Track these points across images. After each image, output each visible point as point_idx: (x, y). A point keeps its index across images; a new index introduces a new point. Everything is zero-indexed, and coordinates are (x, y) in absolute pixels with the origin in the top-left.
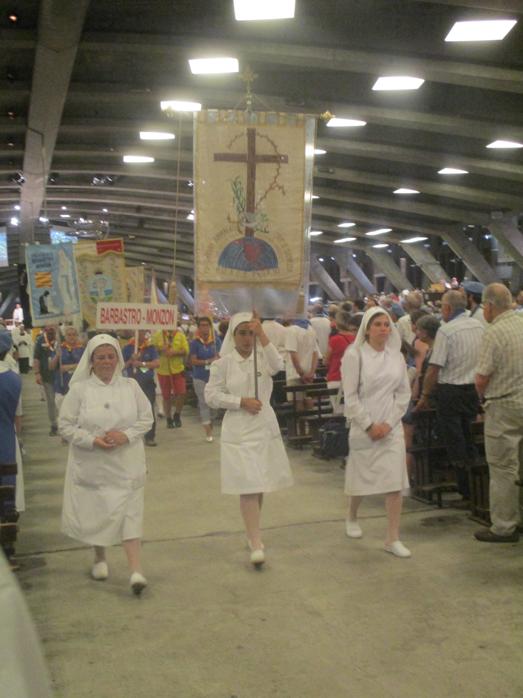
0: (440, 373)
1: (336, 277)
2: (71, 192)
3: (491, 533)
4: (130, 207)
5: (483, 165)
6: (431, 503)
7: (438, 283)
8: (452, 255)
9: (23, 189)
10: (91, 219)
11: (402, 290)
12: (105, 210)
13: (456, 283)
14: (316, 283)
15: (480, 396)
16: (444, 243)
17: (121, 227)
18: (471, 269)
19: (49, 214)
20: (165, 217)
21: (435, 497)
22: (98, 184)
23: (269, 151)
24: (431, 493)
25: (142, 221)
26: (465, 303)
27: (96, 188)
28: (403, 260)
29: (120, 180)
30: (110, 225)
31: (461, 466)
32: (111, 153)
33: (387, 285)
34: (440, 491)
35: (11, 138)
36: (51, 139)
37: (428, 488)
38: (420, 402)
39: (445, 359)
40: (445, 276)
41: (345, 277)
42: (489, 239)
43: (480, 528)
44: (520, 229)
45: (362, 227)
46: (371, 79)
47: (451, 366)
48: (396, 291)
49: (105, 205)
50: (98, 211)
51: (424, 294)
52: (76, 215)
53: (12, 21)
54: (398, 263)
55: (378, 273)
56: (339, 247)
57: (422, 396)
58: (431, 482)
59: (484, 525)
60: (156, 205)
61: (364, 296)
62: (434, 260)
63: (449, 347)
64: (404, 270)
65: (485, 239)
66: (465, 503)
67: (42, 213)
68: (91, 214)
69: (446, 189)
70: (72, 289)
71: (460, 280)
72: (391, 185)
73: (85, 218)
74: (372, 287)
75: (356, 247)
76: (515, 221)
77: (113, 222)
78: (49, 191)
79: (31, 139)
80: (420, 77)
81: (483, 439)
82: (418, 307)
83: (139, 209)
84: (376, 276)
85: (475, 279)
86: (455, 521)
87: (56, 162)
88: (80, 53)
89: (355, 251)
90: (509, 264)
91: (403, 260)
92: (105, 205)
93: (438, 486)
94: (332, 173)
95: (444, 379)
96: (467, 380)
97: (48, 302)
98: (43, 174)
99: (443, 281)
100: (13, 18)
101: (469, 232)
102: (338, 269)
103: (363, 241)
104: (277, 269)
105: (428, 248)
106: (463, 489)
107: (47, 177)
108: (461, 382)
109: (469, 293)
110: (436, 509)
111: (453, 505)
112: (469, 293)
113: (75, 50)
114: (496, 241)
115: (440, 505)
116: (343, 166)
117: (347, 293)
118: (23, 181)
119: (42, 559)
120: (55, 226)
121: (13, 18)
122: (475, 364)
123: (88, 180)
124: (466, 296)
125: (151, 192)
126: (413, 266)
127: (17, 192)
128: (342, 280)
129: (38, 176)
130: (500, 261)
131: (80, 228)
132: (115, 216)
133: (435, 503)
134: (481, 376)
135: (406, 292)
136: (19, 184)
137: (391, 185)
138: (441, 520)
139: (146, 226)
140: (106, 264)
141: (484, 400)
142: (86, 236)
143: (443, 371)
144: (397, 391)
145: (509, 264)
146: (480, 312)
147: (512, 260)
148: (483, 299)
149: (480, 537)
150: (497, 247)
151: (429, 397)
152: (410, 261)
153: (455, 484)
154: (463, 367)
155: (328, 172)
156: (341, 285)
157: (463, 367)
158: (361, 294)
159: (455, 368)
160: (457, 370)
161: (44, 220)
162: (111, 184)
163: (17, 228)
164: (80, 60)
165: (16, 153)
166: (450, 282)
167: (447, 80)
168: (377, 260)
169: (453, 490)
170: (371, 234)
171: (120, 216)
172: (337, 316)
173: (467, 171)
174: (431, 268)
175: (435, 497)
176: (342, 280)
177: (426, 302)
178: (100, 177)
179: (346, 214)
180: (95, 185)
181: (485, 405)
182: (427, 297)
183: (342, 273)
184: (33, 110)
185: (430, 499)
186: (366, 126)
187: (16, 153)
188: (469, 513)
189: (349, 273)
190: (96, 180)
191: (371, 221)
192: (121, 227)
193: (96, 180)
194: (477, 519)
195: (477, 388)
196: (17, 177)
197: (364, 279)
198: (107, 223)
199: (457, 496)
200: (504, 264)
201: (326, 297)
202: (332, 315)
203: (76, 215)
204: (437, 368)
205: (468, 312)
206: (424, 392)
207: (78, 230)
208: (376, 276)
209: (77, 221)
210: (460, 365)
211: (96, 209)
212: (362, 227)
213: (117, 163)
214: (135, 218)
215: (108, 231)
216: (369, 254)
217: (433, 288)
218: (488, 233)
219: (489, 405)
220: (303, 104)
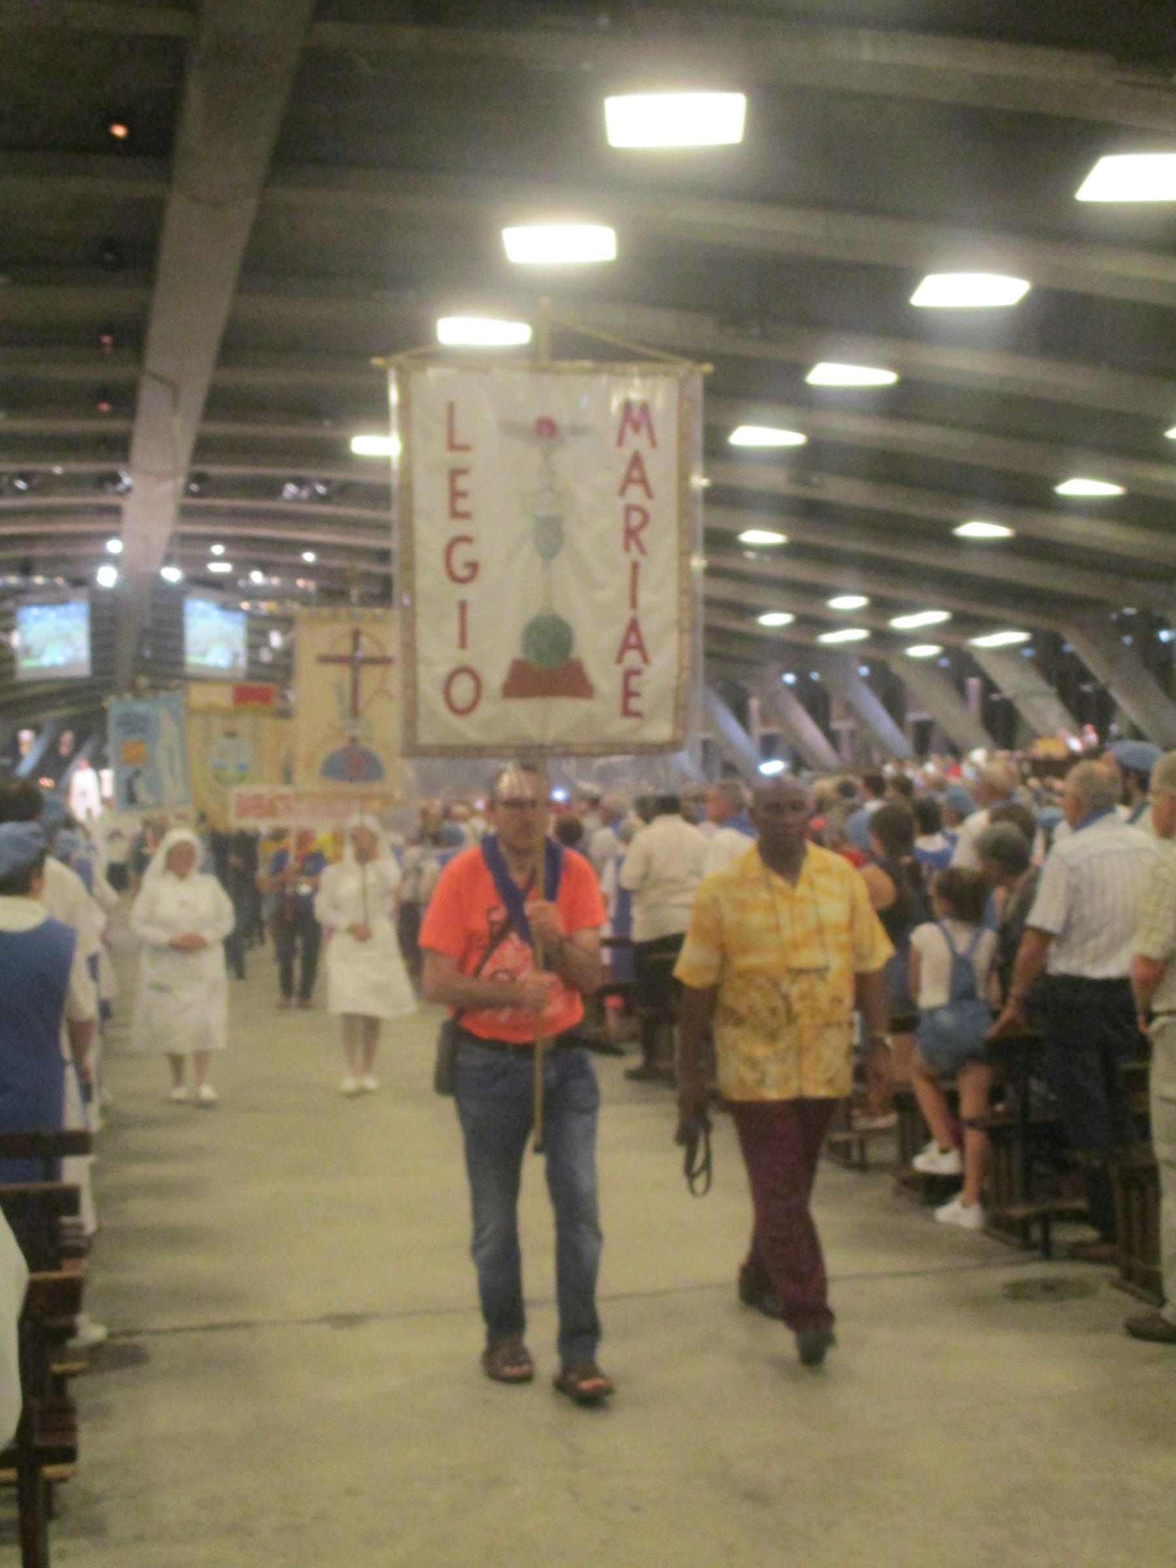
0: (1052, 949)
2: (235, 515)
3: (1163, 1321)
6: (1027, 1246)
7: (1052, 735)
8: (1085, 675)
9: (130, 506)
10: (279, 574)
11: (970, 748)
13: (1092, 737)
14: (774, 729)
15: (1139, 1005)
18: (1128, 709)
19: (183, 562)
21: (1036, 1234)
22: (296, 499)
23: (375, 652)
24: (1025, 1223)
26: (1118, 791)
28: (974, 683)
29: (342, 492)
31: (1097, 1163)
32: (325, 430)
33: (935, 739)
34: (1046, 1220)
35: (104, 393)
36: (195, 397)
37: (1019, 1211)
38: (1008, 1013)
39: (1061, 917)
40: (1068, 721)
41: (841, 718)
43: (1137, 1308)
45: (882, 607)
46: (907, 279)
47: (1075, 937)
48: (956, 752)
51: (1020, 762)
52: (243, 566)
53: (114, 139)
54: (961, 688)
57: (1011, 1002)
58: (1028, 1196)
59: (1151, 1303)
61: (884, 762)
62: (1041, 685)
63: (1073, 890)
64: (975, 705)
65: (1157, 641)
66: (1106, 1250)
67: (168, 560)
69: (1074, 529)
70: (179, 766)
71: (1103, 733)
72: (946, 514)
74: (902, 743)
78: (186, 513)
79: (150, 397)
80: (1021, 273)
81: (1146, 1103)
82: (1007, 795)
84: (913, 716)
85: (1137, 734)
86: (1082, 1289)
87: (204, 448)
88: (262, 208)
89: (866, 661)
91: (974, 683)
93: (1045, 1207)
95: (1061, 964)
96: (1113, 968)
97: (140, 787)
98: (172, 475)
99: (1062, 732)
100: (119, 131)
101: (1125, 625)
103: (884, 639)
105: (1033, 660)
106: (1098, 1217)
107: (181, 480)
108: (1098, 972)
109: (1126, 771)
110: (1040, 1260)
111: (1077, 1253)
112: (1126, 771)
115: (1047, 1251)
116: (845, 472)
117: (846, 754)
118: (129, 490)
119: (136, 1348)
120: (197, 590)
121: (119, 131)
122: (1134, 929)
123: (272, 488)
124: (1118, 775)
126: (995, 697)
127: (115, 512)
129: (161, 477)
131: (254, 594)
133: (1034, 1247)
134: (1146, 961)
135: (978, 755)
136: (120, 494)
137: (946, 514)
138: (1050, 1288)
140: (244, 724)
141: (1151, 1017)
143: (1059, 946)
146: (1147, 816)
148: (1155, 782)
149: (1138, 1331)
151: (1027, 1004)
152: (989, 686)
153: (1081, 1204)
154: (1104, 939)
155: (805, 483)
156: (832, 737)
157: (1104, 939)
158: (876, 757)
159: (1085, 940)
160: (1091, 944)
161: (172, 575)
162: (323, 499)
163: (111, 593)
164: (259, 226)
165: (114, 426)
166: (1080, 734)
167: (1079, 285)
168: (914, 682)
169: (1079, 1217)
170: (902, 623)
174: (1038, 702)
175: (1036, 1234)
177: (1024, 779)
178: (300, 482)
179: (847, 577)
180: (288, 501)
181: (1156, 1025)
182: (1026, 768)
183: (836, 710)
184: (157, 331)
185: (1026, 1236)
187: (114, 426)
188: (1114, 1272)
189: (850, 710)
190: (290, 489)
191: (903, 594)
193: (290, 489)
194: (1131, 1286)
195: (1136, 988)
196: (115, 479)
197: (883, 723)
199: (1089, 1234)
203: (243, 566)
204: (1044, 937)
205: (1123, 812)
206: (1016, 990)
208: (913, 716)
209: (247, 578)
210: (1096, 934)
212: (882, 607)
213: (335, 453)
216: (896, 668)
217: (1043, 748)
218: (1166, 626)
219: (1163, 1027)
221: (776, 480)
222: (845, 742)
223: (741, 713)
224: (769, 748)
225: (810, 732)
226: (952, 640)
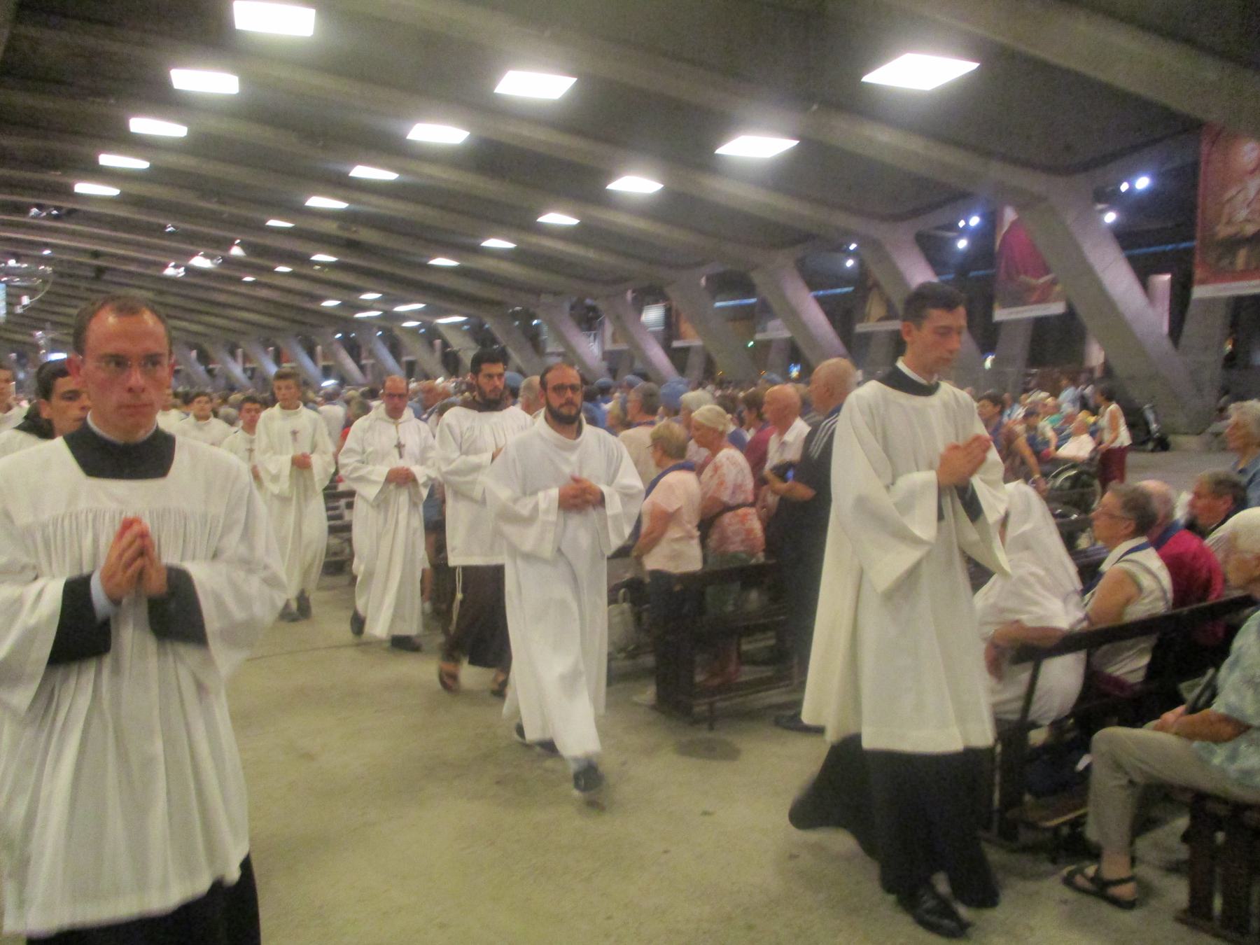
1: (356, 356)
4: (85, 251)
5: (534, 240)
8: (494, 341)
12: (249, 279)
14: (330, 363)
16: (487, 326)
17: (70, 276)
20: (133, 268)
22: (36, 217)
25: (100, 271)
27: (32, 221)
28: (438, 342)
30: (54, 272)
33: (417, 369)
42: (537, 325)
44: (571, 315)
49: (47, 245)
50: (36, 253)
54: (431, 345)
55: (407, 355)
56: (361, 322)
60: (150, 258)
64: (438, 354)
68: (26, 256)
73: (18, 258)
75: (383, 323)
76: (567, 306)
77: (59, 269)
83: (96, 254)
84: (405, 359)
88: (13, 38)
90: (559, 355)
91: (438, 342)
92: (47, 245)
94: (355, 232)
101: (515, 316)
102: (359, 347)
103: (390, 317)
104: (147, 558)
113: (6, 32)
114: (545, 328)
123: (22, 209)
125: (113, 234)
128: (364, 362)
130: (549, 350)
132: (61, 261)
139: (107, 277)
142: (18, 284)
144: (453, 549)
145: (559, 355)
147: (561, 350)
148: (521, 392)
150: (546, 335)
152: (445, 344)
156: (362, 368)
162: (57, 218)
168: (406, 340)
171: (69, 262)
172: (353, 403)
173: (514, 243)
176: (364, 362)
178: (39, 207)
183: (364, 354)
186: (715, 151)
189: (371, 354)
190: (34, 211)
192: (70, 276)
193: (34, 211)
197: (390, 361)
198: (49, 269)
200: (552, 354)
201: (344, 381)
202: (348, 402)
207: (7, 275)
208: (405, 359)
211: (31, 249)
213: (68, 193)
214: (90, 266)
215: (51, 280)
216: (397, 332)
218: (534, 317)
220: (321, 143)
221: (331, 227)
222: (369, 372)
223: (311, 354)
224: (327, 372)
225: (349, 364)
226: (386, 307)
